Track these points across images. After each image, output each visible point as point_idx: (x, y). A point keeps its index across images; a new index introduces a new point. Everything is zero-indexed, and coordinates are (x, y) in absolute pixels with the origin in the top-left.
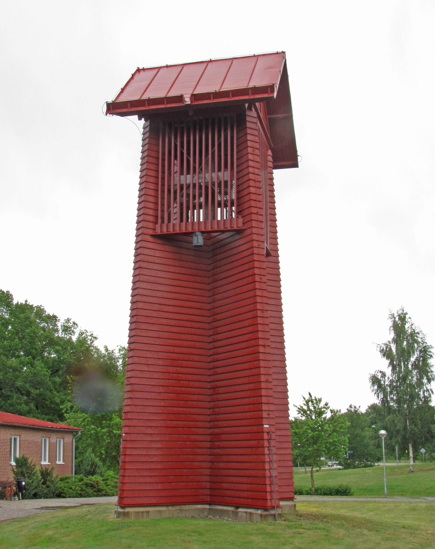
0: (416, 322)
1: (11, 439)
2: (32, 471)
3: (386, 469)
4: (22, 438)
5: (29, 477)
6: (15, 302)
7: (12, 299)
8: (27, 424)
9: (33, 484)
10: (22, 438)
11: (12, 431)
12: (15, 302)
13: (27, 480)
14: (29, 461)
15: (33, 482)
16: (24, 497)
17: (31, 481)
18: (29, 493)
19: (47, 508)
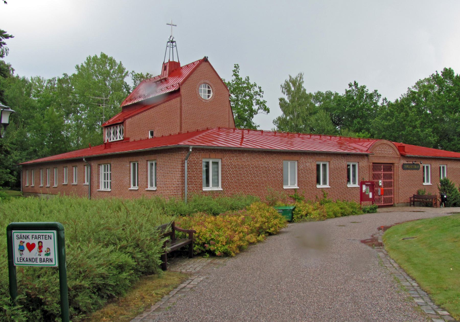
0: (122, 63)
1: (440, 167)
2: (452, 188)
3: (436, 203)
4: (448, 167)
5: (449, 192)
6: (455, 75)
7: (453, 73)
8: (451, 157)
9: (453, 197)
10: (448, 167)
11: (441, 162)
12: (455, 75)
13: (448, 194)
14: (450, 181)
15: (452, 196)
16: (446, 206)
17: (450, 195)
18: (450, 203)
19: (454, 213)
